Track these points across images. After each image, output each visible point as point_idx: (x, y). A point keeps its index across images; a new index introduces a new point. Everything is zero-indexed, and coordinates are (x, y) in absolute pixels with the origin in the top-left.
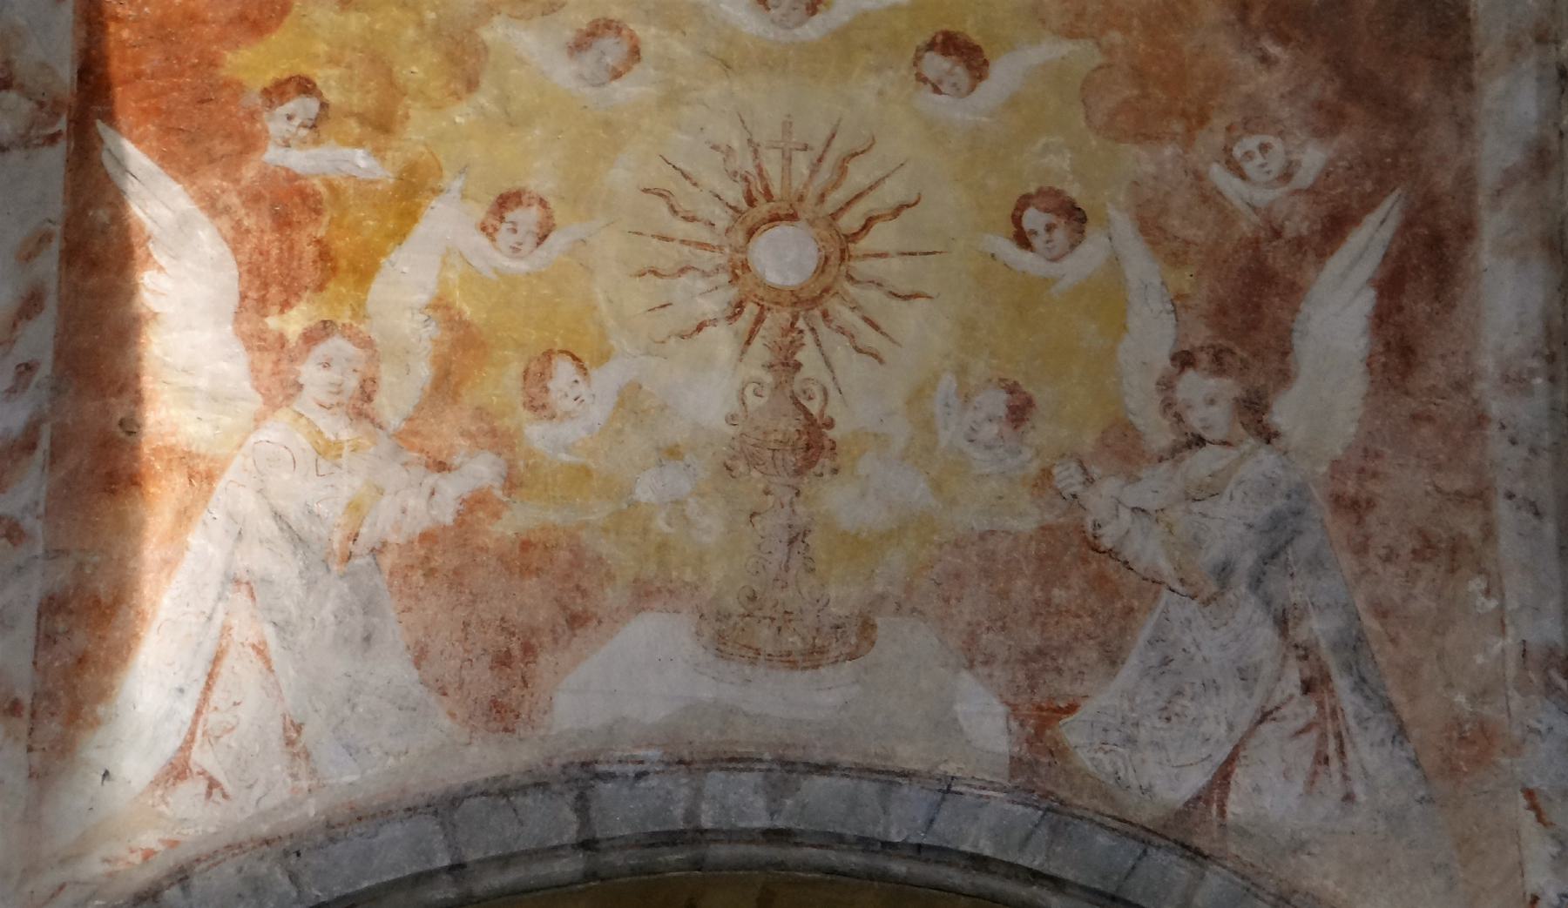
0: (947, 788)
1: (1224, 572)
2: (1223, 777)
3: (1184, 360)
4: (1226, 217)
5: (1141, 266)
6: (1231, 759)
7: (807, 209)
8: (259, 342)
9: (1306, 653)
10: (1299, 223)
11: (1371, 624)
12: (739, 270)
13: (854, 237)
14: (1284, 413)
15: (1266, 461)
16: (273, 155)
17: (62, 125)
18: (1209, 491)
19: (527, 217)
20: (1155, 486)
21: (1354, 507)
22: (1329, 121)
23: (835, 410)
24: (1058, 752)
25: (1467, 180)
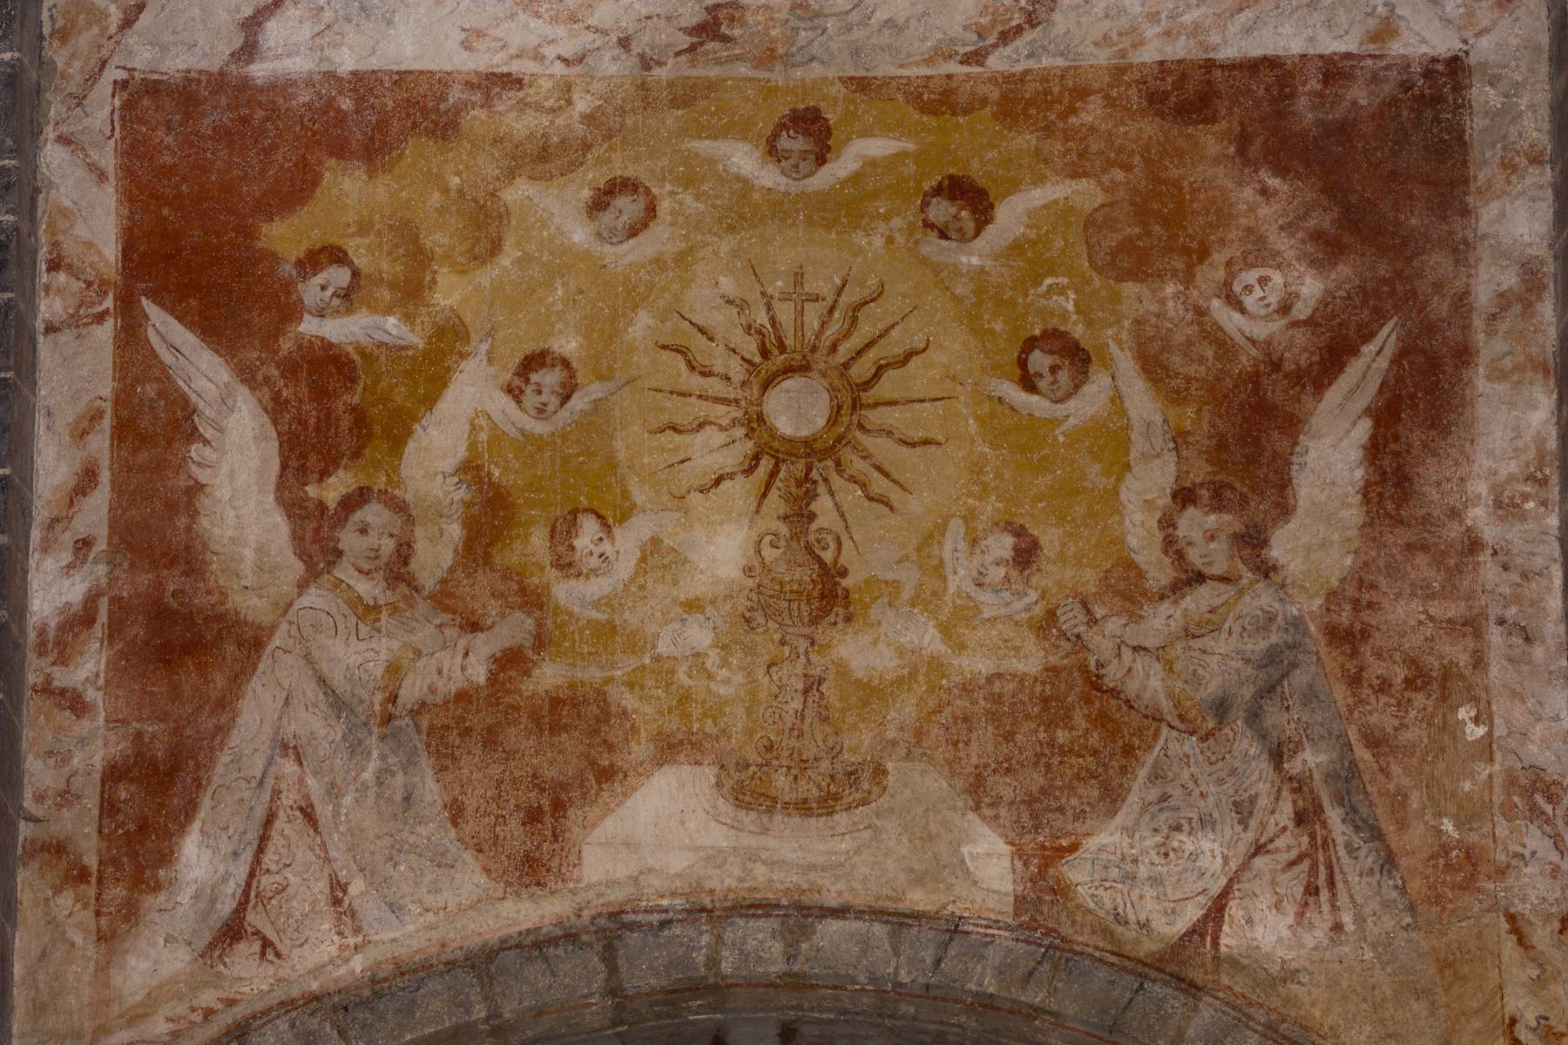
0: (954, 929)
1: (1221, 708)
2: (1217, 910)
3: (1184, 496)
4: (1224, 345)
5: (1142, 402)
6: (1225, 894)
7: (819, 361)
8: (296, 508)
9: (1299, 785)
10: (1299, 349)
11: (1362, 754)
12: (756, 422)
13: (867, 385)
14: (1280, 548)
15: (1262, 598)
16: (309, 326)
17: (109, 303)
18: (1209, 625)
19: (549, 378)
20: (1161, 620)
21: (1346, 638)
22: (1326, 250)
23: (848, 557)
24: (1062, 891)
25: (1462, 301)
